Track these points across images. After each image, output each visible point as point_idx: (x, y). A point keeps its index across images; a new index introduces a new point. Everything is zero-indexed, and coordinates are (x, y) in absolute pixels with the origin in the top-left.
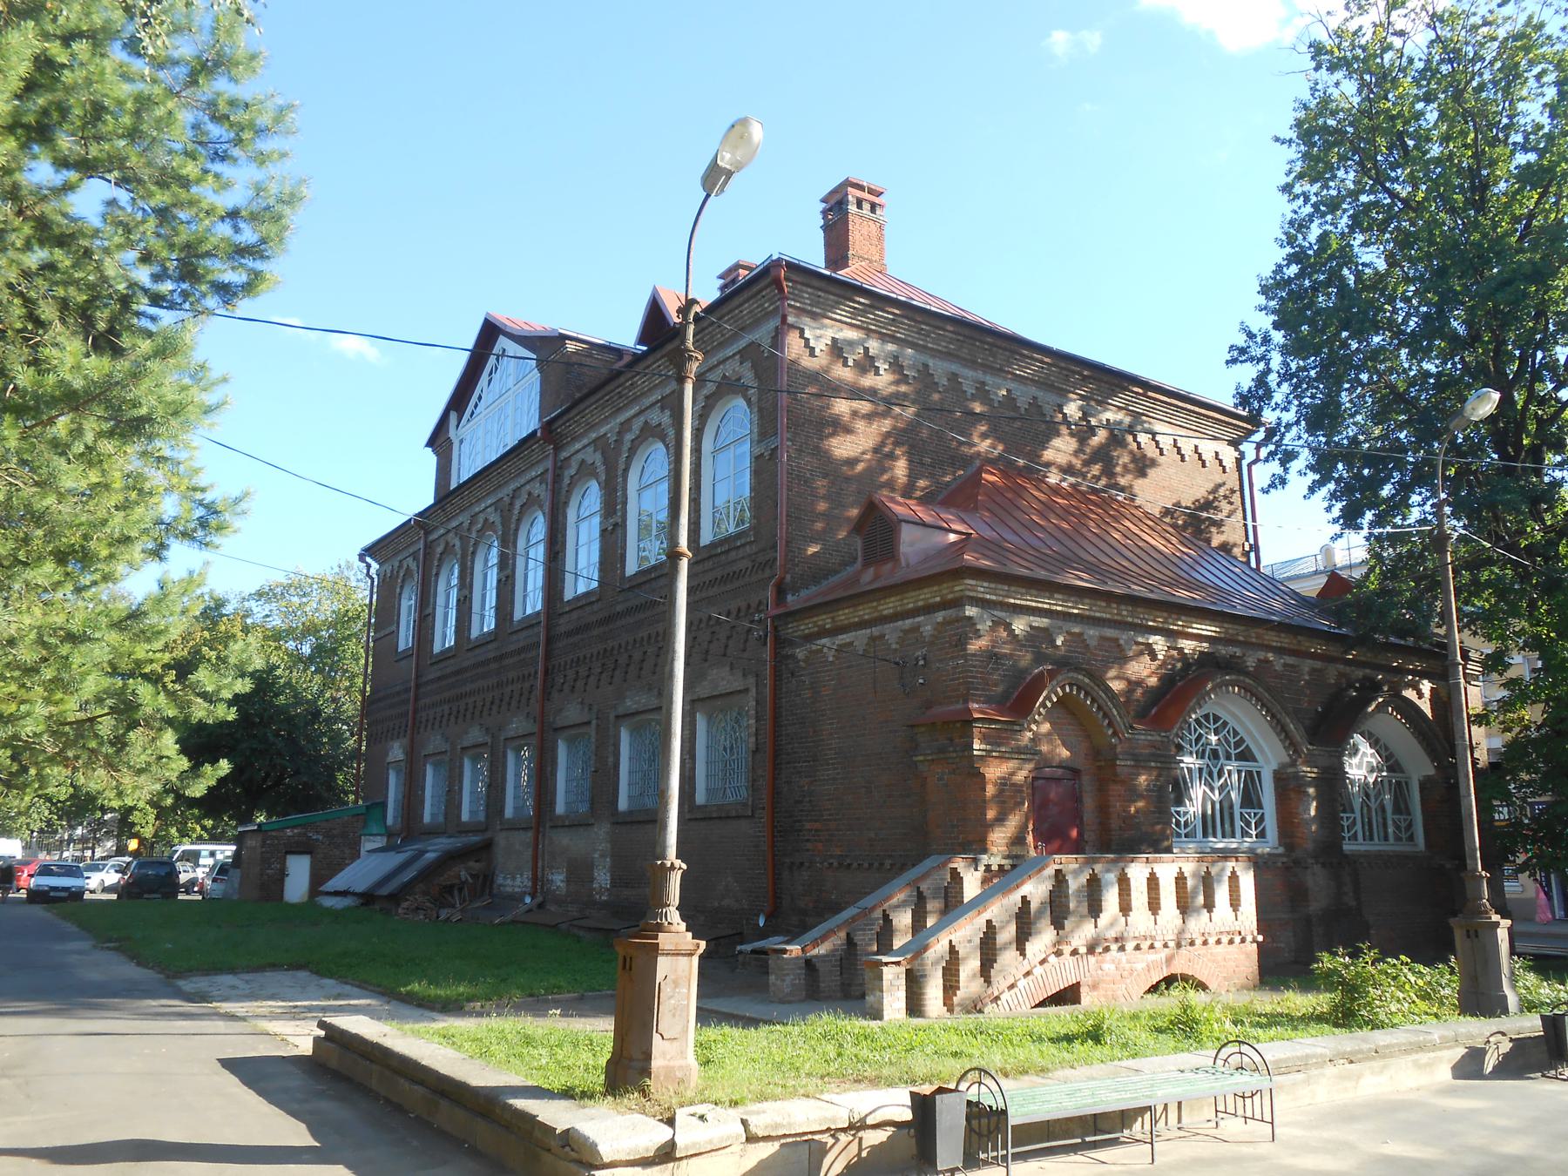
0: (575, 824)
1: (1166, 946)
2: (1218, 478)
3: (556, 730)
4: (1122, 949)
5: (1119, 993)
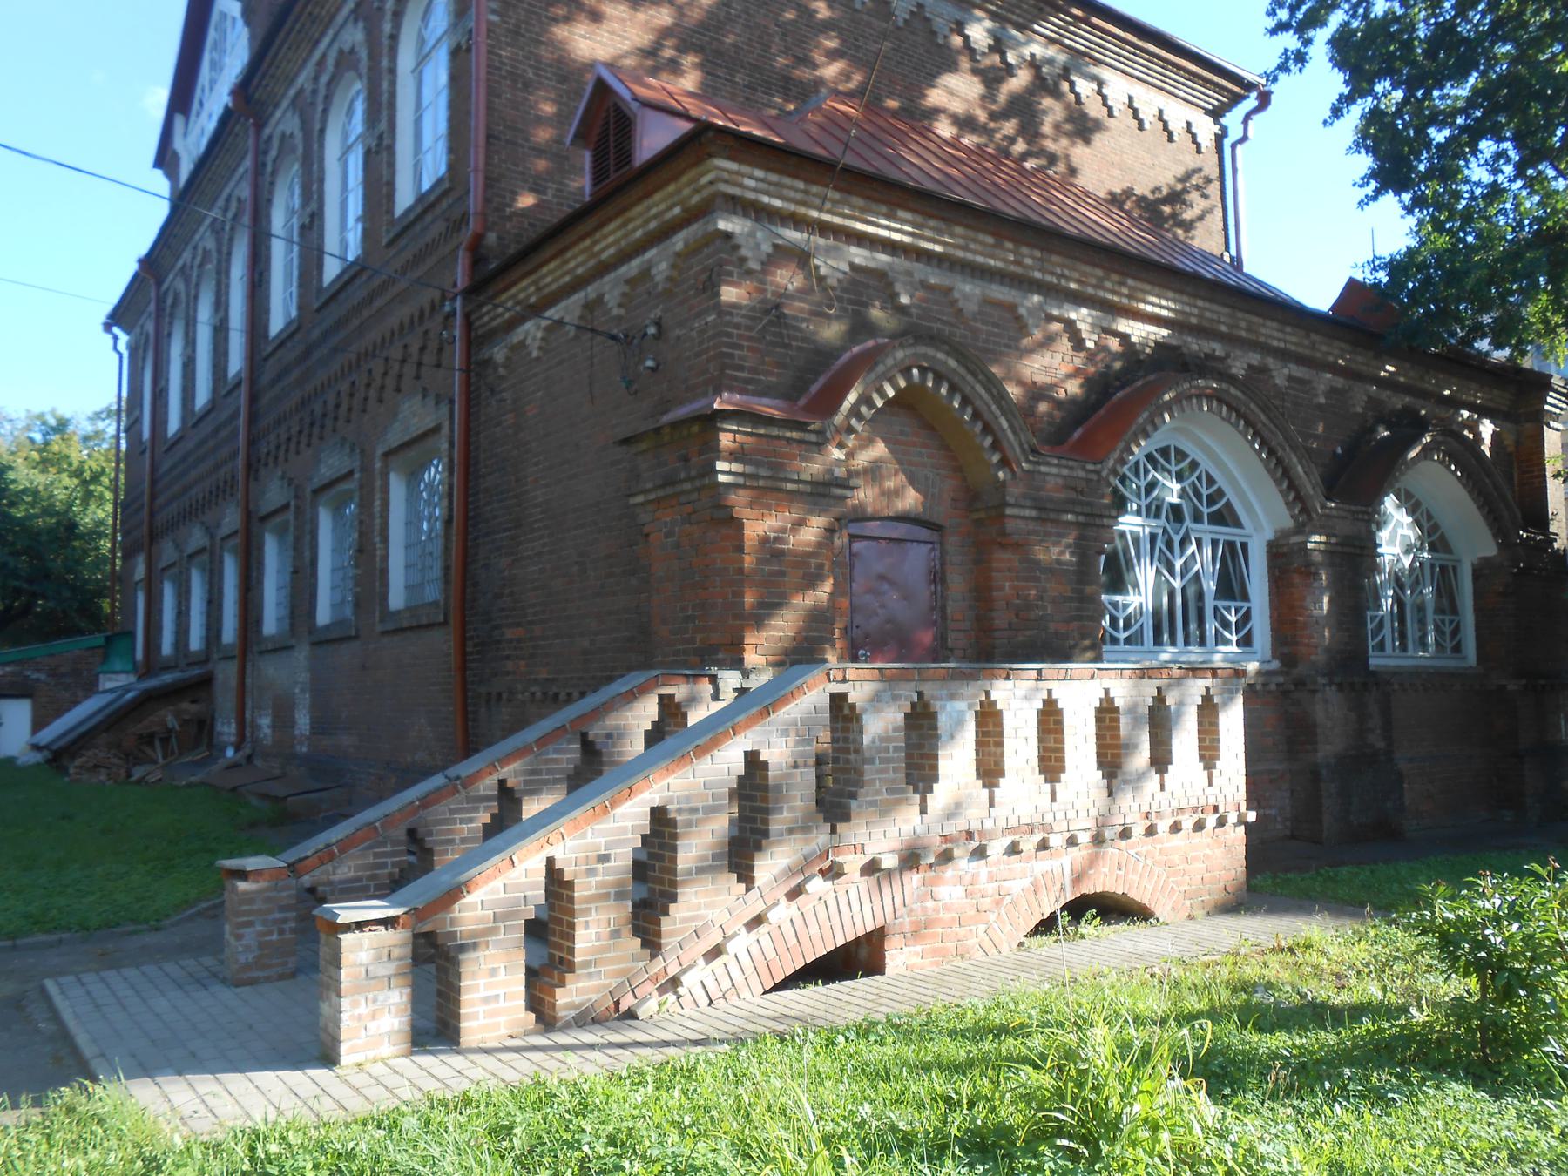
0: (281, 648)
1: (1072, 842)
2: (1191, 161)
3: (264, 519)
4: (980, 853)
5: (972, 942)
